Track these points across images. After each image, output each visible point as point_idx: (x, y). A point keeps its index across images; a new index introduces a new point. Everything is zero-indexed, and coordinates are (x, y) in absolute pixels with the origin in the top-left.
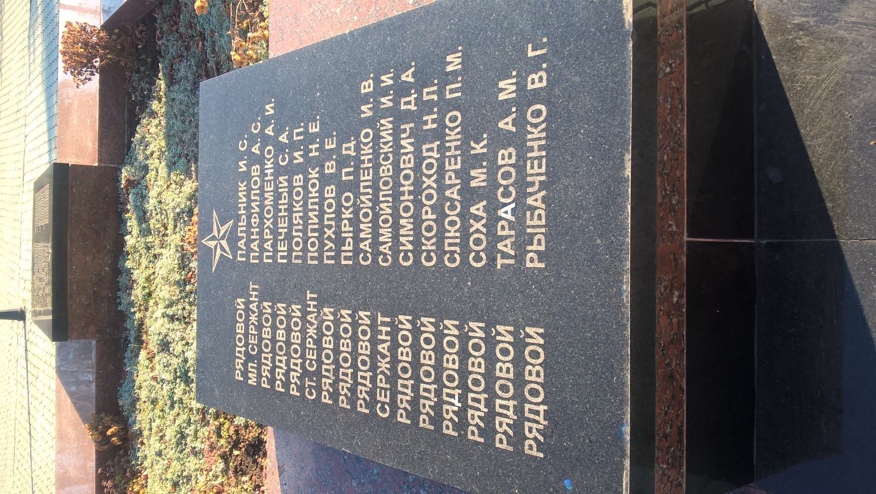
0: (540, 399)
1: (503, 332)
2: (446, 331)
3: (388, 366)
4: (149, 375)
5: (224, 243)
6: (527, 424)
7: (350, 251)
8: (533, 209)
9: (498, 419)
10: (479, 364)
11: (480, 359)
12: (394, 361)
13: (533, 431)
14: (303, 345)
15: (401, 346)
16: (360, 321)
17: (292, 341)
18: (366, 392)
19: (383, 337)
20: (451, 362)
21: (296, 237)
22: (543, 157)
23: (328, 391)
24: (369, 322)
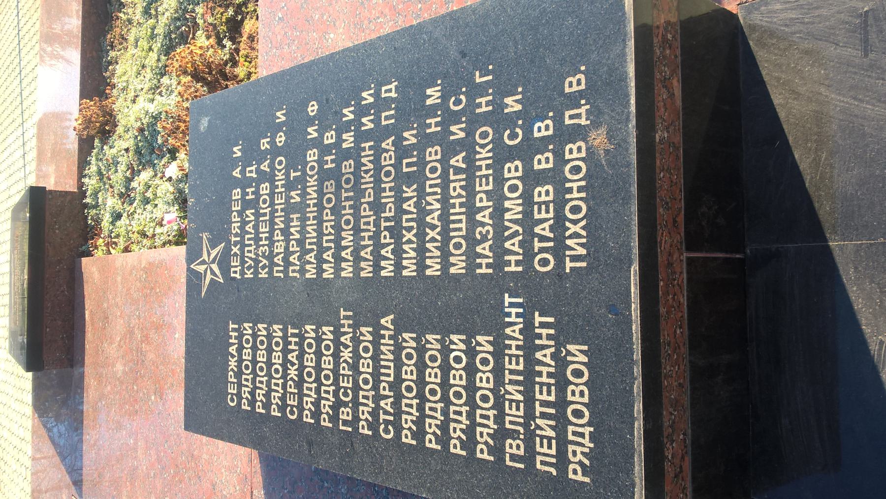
1: (407, 339)
5: (215, 267)
6: (479, 429)
10: (488, 379)
12: (240, 361)
13: (578, 454)
15: (454, 368)
17: (258, 359)
19: (346, 329)
20: (458, 378)
22: (490, 175)
23: (310, 410)
24: (371, 338)
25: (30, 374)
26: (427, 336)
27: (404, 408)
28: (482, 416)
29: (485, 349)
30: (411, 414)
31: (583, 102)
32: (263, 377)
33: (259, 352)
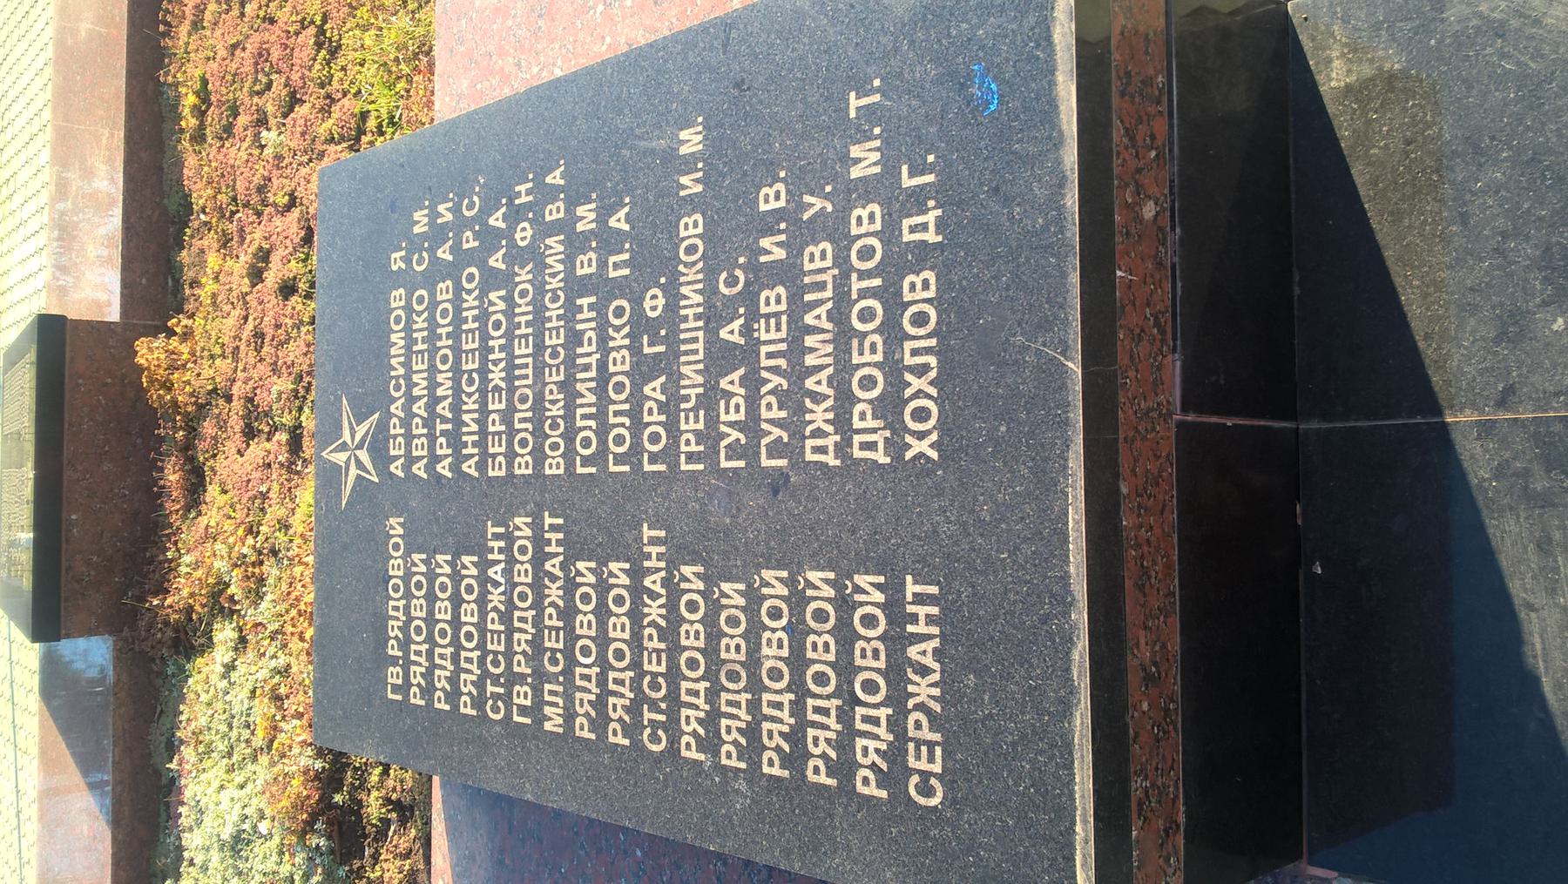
0: (878, 698)
2: (765, 591)
3: (936, 692)
4: (221, 690)
5: (363, 455)
6: (811, 732)
7: (781, 341)
8: (729, 395)
9: (860, 743)
11: (875, 644)
14: (636, 641)
16: (579, 579)
18: (781, 734)
19: (920, 628)
21: (585, 428)
23: (735, 743)
24: (627, 582)
25: (37, 645)
26: (856, 577)
27: (685, 698)
28: (817, 710)
29: (693, 587)
30: (876, 737)
31: (931, 203)
32: (471, 650)
33: (613, 620)
